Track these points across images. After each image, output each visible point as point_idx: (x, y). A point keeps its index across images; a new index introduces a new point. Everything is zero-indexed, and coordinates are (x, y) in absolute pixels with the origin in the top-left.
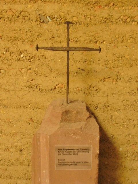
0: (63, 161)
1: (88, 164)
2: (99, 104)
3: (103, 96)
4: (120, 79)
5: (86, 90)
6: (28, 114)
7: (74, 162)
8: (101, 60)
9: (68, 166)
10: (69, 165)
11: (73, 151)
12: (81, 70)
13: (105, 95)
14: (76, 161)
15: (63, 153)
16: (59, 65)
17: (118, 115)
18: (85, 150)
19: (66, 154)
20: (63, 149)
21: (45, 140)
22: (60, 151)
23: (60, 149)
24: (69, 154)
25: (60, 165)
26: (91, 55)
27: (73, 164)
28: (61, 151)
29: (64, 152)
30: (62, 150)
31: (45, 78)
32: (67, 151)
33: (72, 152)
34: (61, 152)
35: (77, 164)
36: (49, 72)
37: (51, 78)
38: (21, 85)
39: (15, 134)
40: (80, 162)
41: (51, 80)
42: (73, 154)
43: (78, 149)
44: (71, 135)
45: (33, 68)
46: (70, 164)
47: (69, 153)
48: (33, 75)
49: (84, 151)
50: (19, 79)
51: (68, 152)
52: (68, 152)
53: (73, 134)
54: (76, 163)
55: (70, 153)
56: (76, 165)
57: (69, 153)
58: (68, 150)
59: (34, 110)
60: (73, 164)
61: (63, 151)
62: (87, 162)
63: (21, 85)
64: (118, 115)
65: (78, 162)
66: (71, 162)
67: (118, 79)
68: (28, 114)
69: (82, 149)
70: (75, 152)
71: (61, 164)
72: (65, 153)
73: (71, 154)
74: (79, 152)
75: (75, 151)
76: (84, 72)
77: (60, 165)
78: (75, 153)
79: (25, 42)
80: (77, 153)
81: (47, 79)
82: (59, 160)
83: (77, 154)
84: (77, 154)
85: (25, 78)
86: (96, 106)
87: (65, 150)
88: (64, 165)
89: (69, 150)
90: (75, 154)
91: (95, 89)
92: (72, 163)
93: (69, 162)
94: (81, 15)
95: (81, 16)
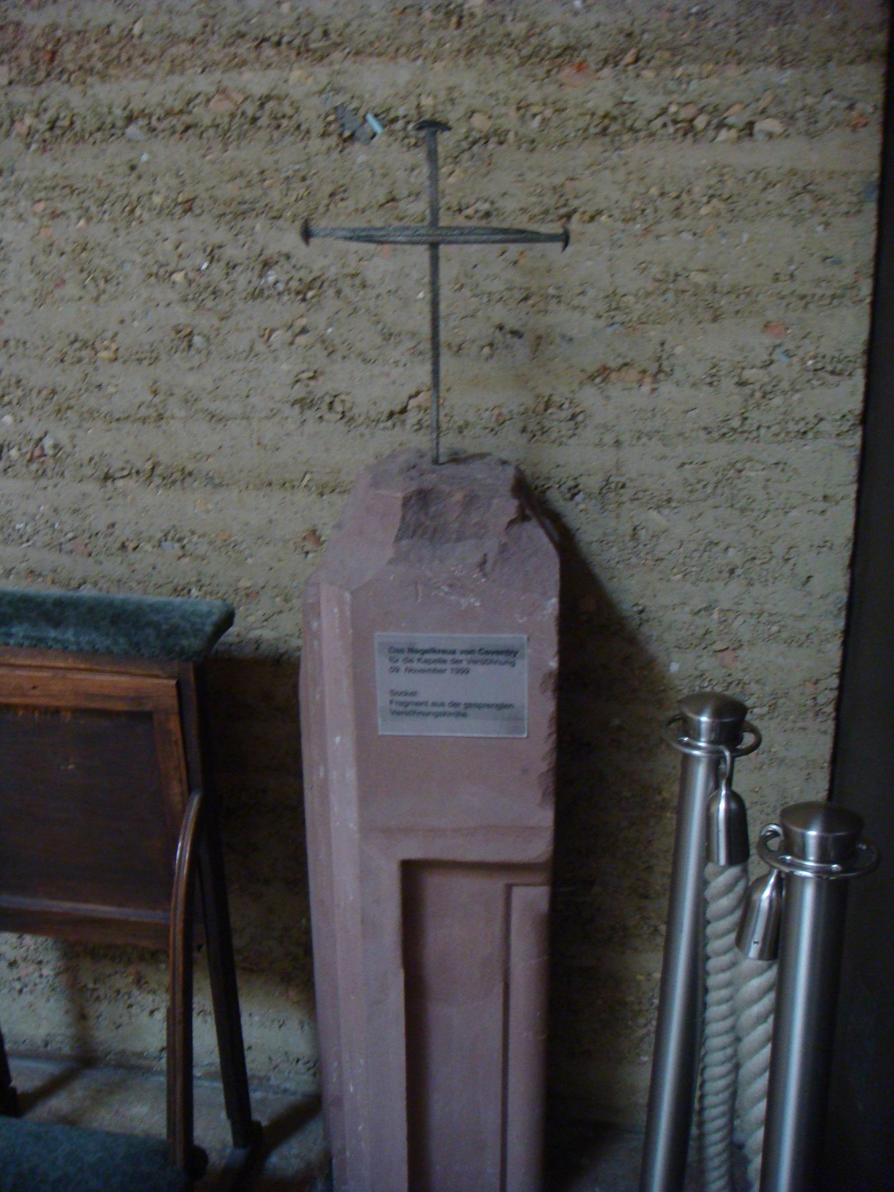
0: (409, 699)
3: (600, 444)
4: (668, 370)
7: (454, 705)
8: (591, 293)
10: (437, 715)
11: (449, 657)
14: (463, 700)
15: (409, 665)
19: (423, 671)
20: (411, 650)
24: (436, 671)
28: (401, 657)
29: (411, 661)
32: (427, 656)
33: (444, 662)
35: (470, 711)
40: (479, 706)
41: (388, 375)
43: (471, 652)
46: (441, 709)
54: (461, 709)
55: (439, 666)
56: (464, 715)
57: (433, 666)
59: (325, 497)
60: (452, 710)
61: (411, 656)
66: (443, 705)
71: (401, 709)
74: (475, 662)
75: (458, 656)
77: (399, 713)
80: (464, 665)
82: (393, 693)
83: (467, 671)
87: (417, 651)
91: (565, 414)
93: (434, 704)
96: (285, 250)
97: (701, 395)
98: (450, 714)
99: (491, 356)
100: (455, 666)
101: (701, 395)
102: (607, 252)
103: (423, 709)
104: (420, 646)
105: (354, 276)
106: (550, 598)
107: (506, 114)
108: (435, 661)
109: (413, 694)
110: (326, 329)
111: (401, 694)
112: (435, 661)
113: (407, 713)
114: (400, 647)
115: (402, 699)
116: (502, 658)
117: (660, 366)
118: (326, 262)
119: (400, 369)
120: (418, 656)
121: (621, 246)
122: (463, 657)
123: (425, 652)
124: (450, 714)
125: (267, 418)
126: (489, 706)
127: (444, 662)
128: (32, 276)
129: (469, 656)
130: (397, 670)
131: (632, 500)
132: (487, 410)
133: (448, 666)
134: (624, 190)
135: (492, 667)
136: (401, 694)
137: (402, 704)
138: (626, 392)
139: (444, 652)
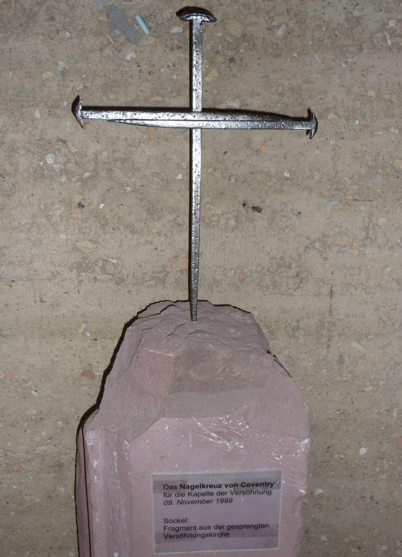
0: (181, 525)
1: (267, 529)
2: (305, 320)
3: (318, 295)
4: (373, 237)
5: (265, 275)
6: (77, 357)
7: (220, 527)
8: (317, 176)
9: (199, 539)
10: (203, 536)
11: (215, 490)
12: (250, 210)
13: (325, 290)
14: (227, 523)
15: (180, 498)
16: (179, 192)
17: (362, 349)
18: (257, 485)
19: (193, 502)
20: (182, 486)
21: (115, 454)
22: (170, 491)
23: (170, 484)
24: (202, 502)
25: (171, 537)
26: (285, 158)
27: (217, 531)
28: (174, 493)
29: (183, 495)
30: (179, 487)
31: (130, 236)
32: (196, 491)
33: (211, 494)
34: (173, 495)
35: (231, 532)
36: (144, 215)
37: (150, 238)
38: (52, 263)
39: (40, 420)
40: (239, 527)
41: (151, 243)
42: (214, 502)
43: (235, 485)
44: (209, 436)
45: (90, 204)
46: (207, 532)
47: (201, 498)
48: (90, 229)
49: (255, 489)
50: (44, 242)
51: (196, 495)
52: (196, 495)
53: (217, 433)
54: (225, 531)
55: (206, 498)
56: (227, 535)
57: (201, 498)
58: (197, 487)
59: (98, 342)
60: (217, 531)
61: (182, 491)
62: (263, 526)
63: (52, 263)
64: (362, 349)
65: (232, 527)
66: (209, 528)
67: (367, 237)
68: (77, 357)
69: (249, 485)
70: (222, 494)
71: (173, 533)
72: (187, 498)
73: (208, 502)
74: (237, 493)
75: (223, 489)
76: (260, 214)
77: (171, 537)
78: (224, 497)
79: (58, 111)
80: (229, 496)
81: (138, 239)
82: (166, 521)
83: (231, 500)
84: (231, 500)
85: (63, 236)
86: (294, 324)
87: (188, 487)
88: (184, 536)
89: (203, 486)
90: (222, 501)
91: (292, 272)
92: (212, 531)
93: (201, 528)
94: (256, 13)
95: (254, 19)
96: (62, 136)
97: (396, 255)
98: (215, 535)
99: (236, 227)
100: (220, 497)
101: (396, 255)
102: (332, 142)
103: (193, 532)
104: (189, 483)
105: (123, 160)
106: (304, 439)
107: (256, 23)
108: (204, 494)
109: (183, 521)
110: (99, 204)
111: (173, 521)
112: (204, 494)
113: (178, 537)
114: (174, 485)
115: (175, 525)
116: (260, 489)
117: (368, 233)
118: (98, 147)
119: (163, 238)
120: (189, 490)
121: (343, 138)
122: (228, 489)
123: (193, 487)
124: (215, 535)
125: (49, 279)
126: (248, 527)
127: (211, 494)
128: (338, 202)
129: (232, 489)
130: (170, 503)
131: (339, 335)
132: (232, 269)
133: (215, 497)
134: (348, 92)
135: (252, 496)
136: (173, 521)
137: (173, 529)
138: (341, 254)
139: (211, 486)
